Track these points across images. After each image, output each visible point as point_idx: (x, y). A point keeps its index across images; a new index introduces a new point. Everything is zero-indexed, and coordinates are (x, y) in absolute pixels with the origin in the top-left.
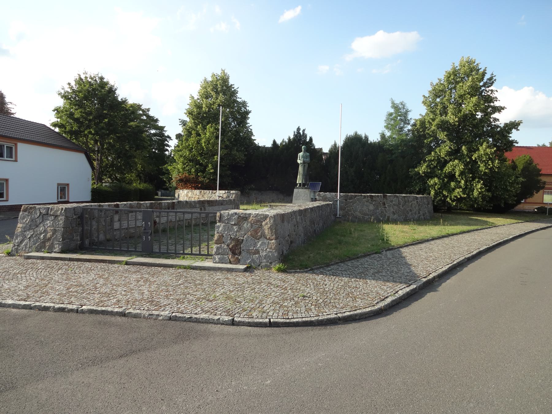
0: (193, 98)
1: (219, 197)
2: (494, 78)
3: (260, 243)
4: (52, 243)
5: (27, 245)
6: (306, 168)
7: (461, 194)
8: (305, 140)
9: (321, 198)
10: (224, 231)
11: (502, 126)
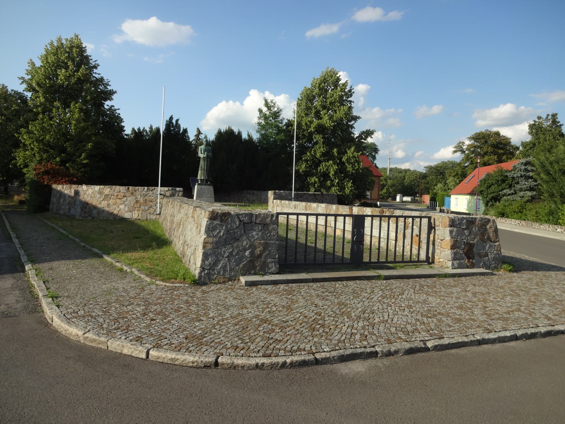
0: (33, 64)
2: (353, 91)
3: (488, 245)
4: (264, 262)
6: (209, 163)
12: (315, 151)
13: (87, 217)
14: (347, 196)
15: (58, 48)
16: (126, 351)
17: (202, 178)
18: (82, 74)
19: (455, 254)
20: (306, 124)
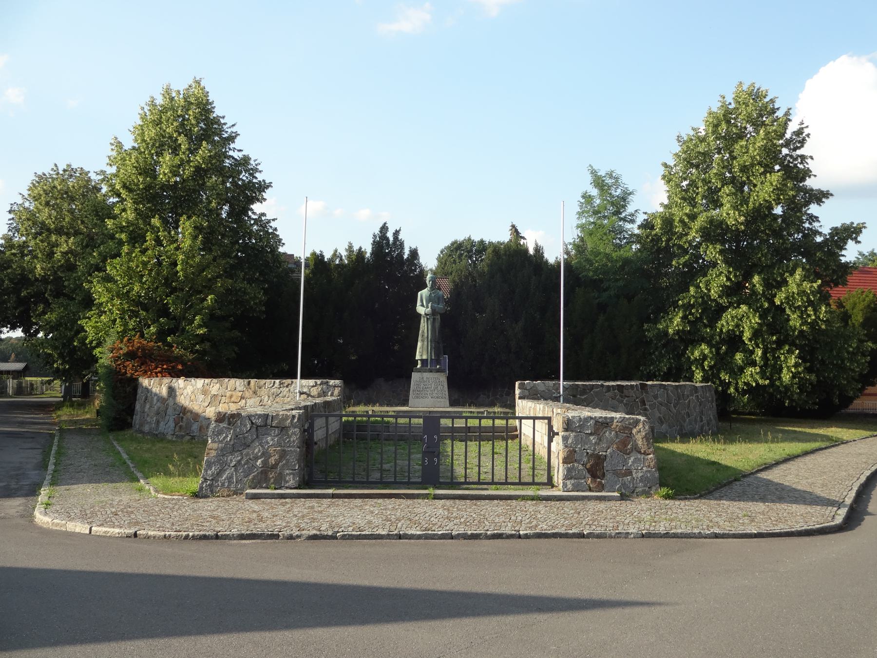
0: (119, 145)
1: (301, 393)
2: (806, 131)
3: (632, 459)
4: (280, 473)
5: (231, 477)
6: (437, 325)
7: (757, 377)
8: (401, 255)
9: (527, 393)
10: (577, 444)
11: (826, 230)
12: (707, 284)
13: (183, 436)
14: (787, 388)
15: (164, 110)
16: (77, 530)
17: (425, 357)
18: (203, 158)
19: (569, 470)
20: (682, 221)
